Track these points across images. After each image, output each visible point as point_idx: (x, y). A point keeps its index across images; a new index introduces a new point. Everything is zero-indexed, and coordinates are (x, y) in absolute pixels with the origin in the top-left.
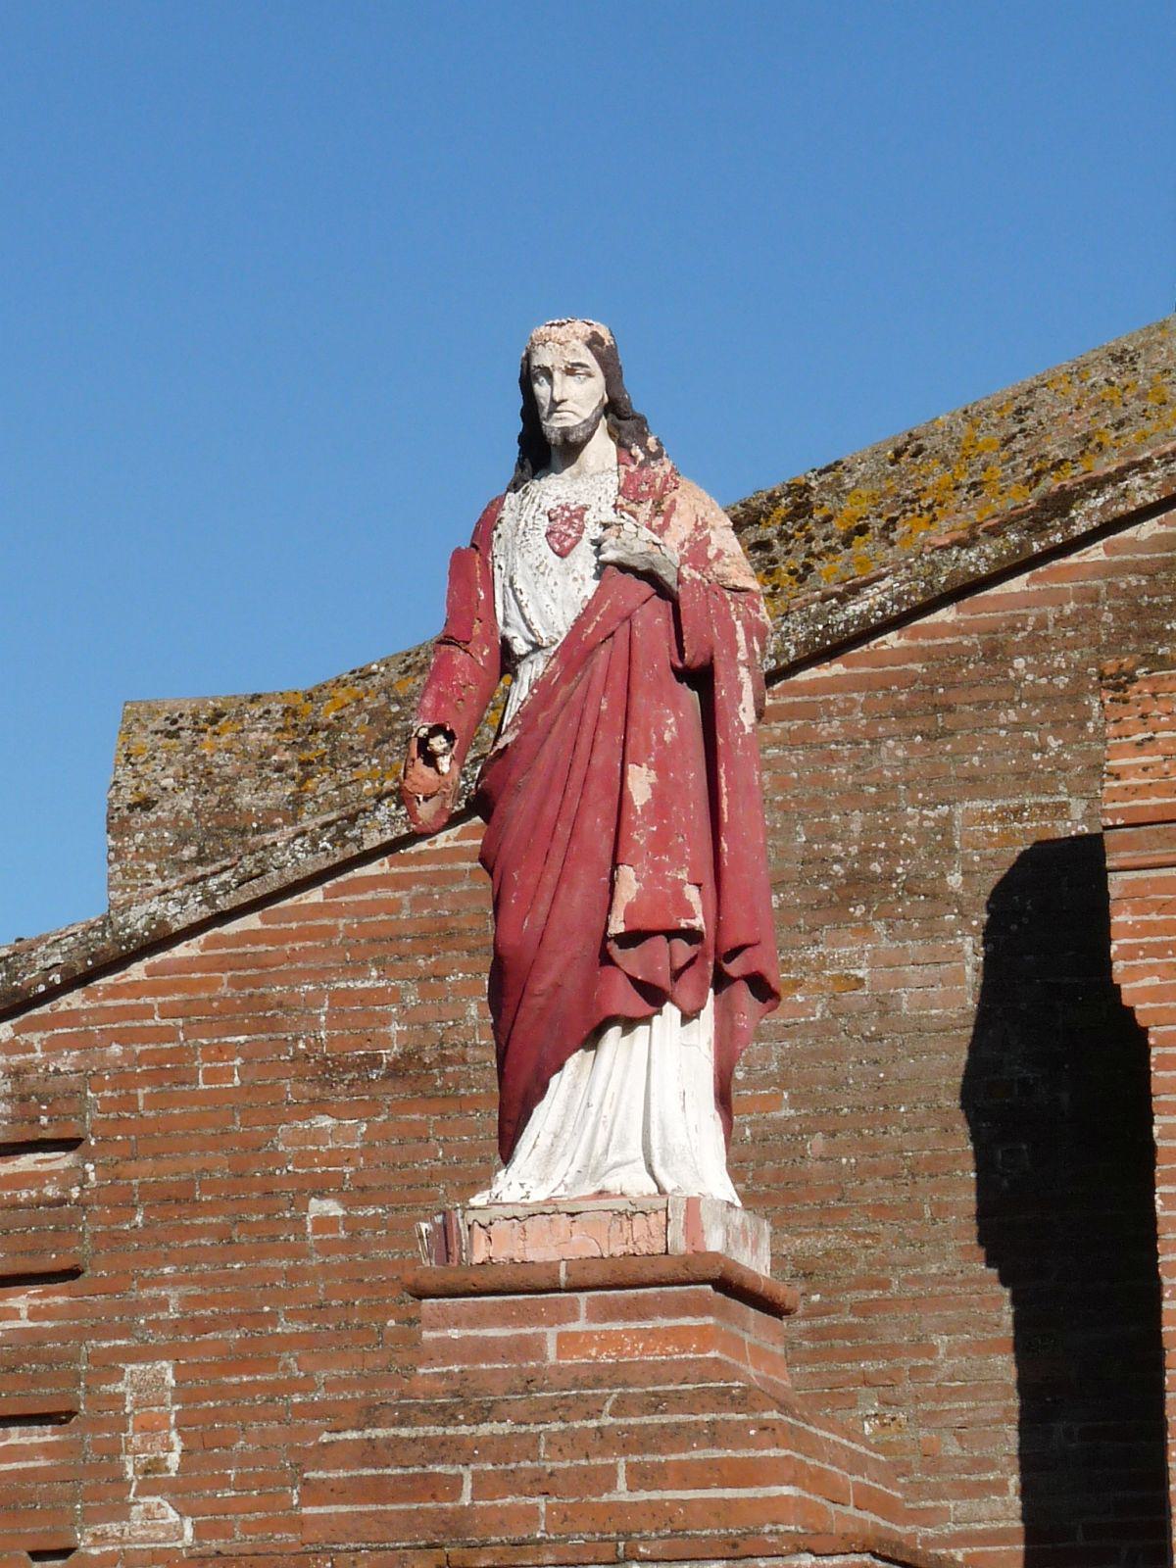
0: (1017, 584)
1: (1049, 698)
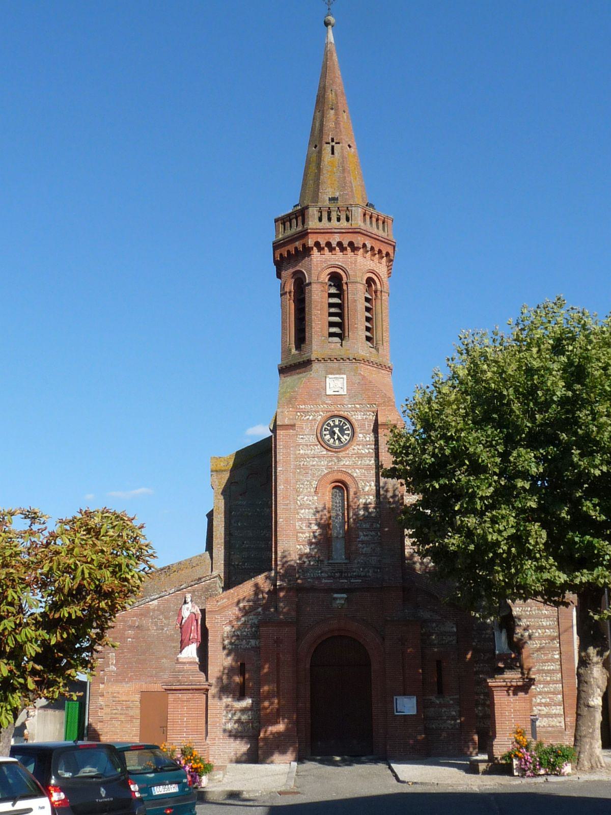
0: (196, 586)
1: (198, 596)
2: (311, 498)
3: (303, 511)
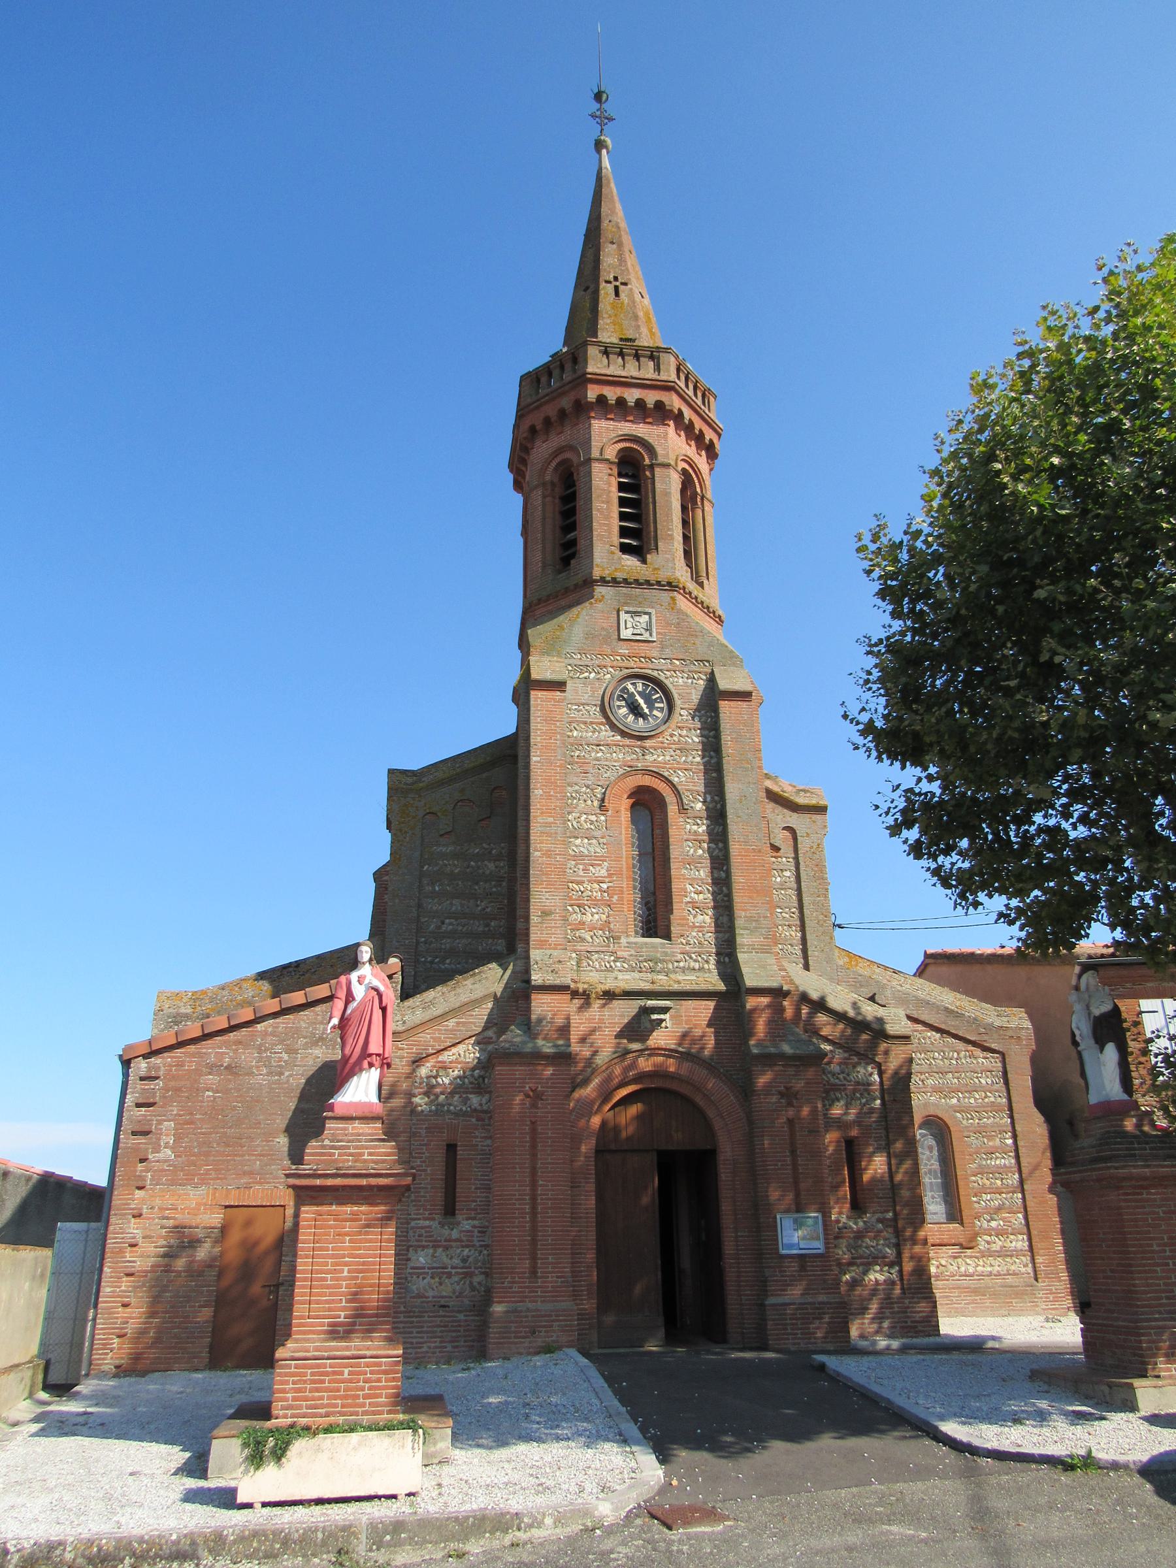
2: (593, 818)
3: (578, 841)
